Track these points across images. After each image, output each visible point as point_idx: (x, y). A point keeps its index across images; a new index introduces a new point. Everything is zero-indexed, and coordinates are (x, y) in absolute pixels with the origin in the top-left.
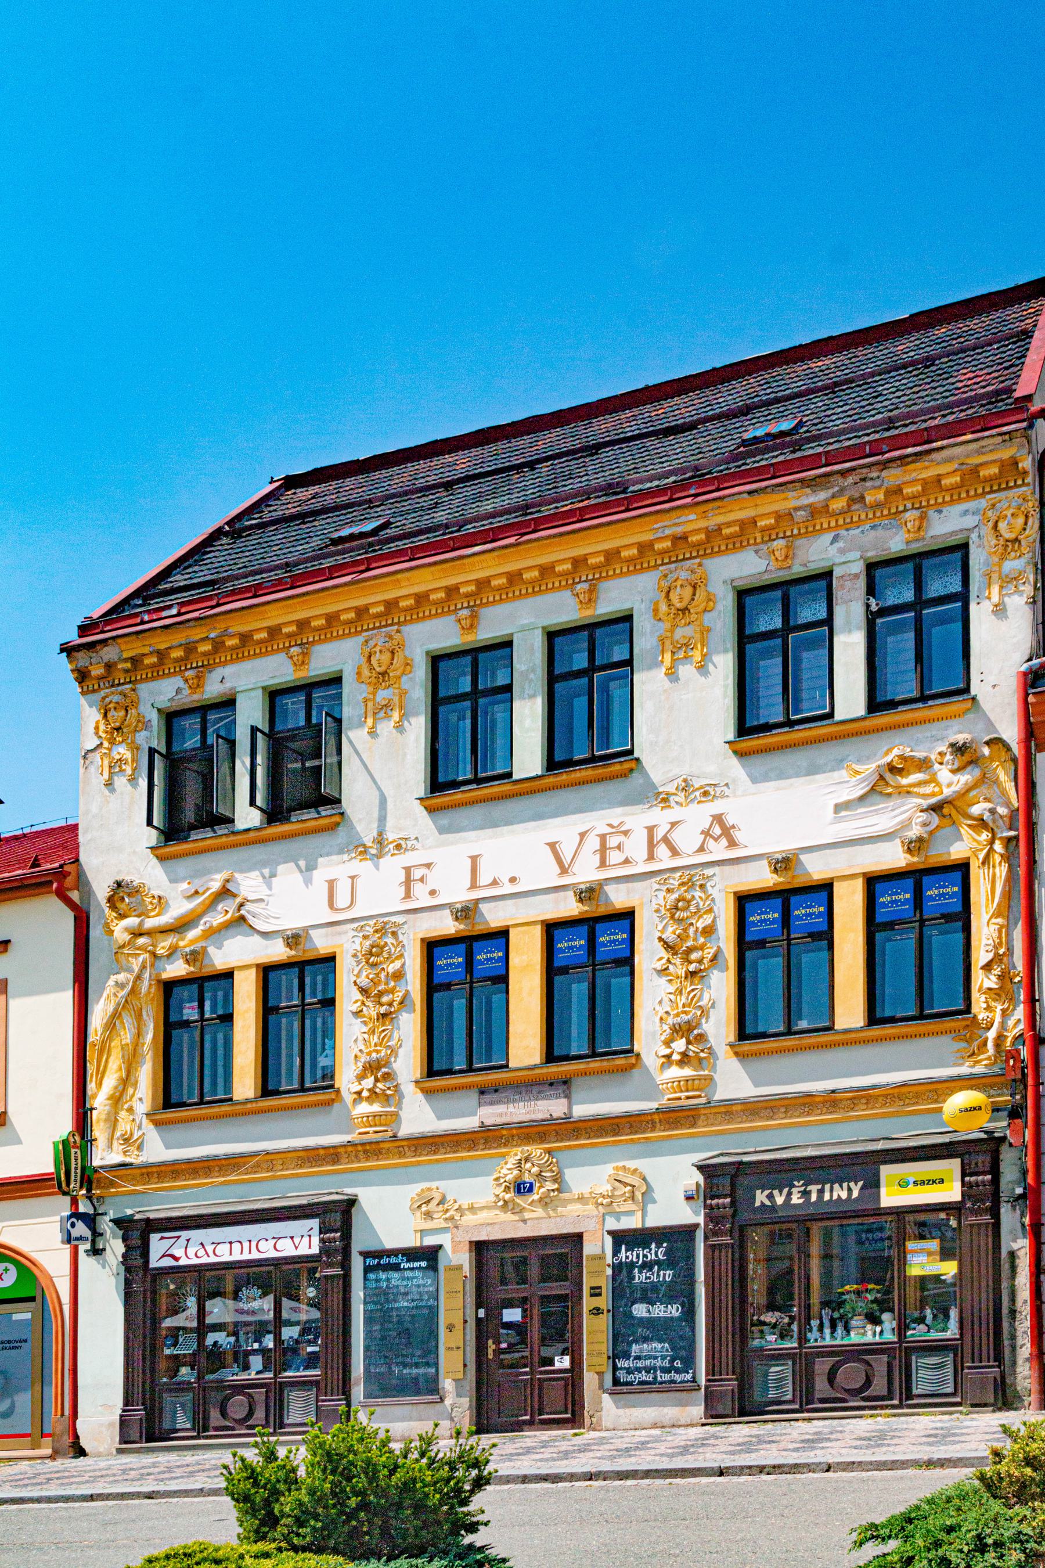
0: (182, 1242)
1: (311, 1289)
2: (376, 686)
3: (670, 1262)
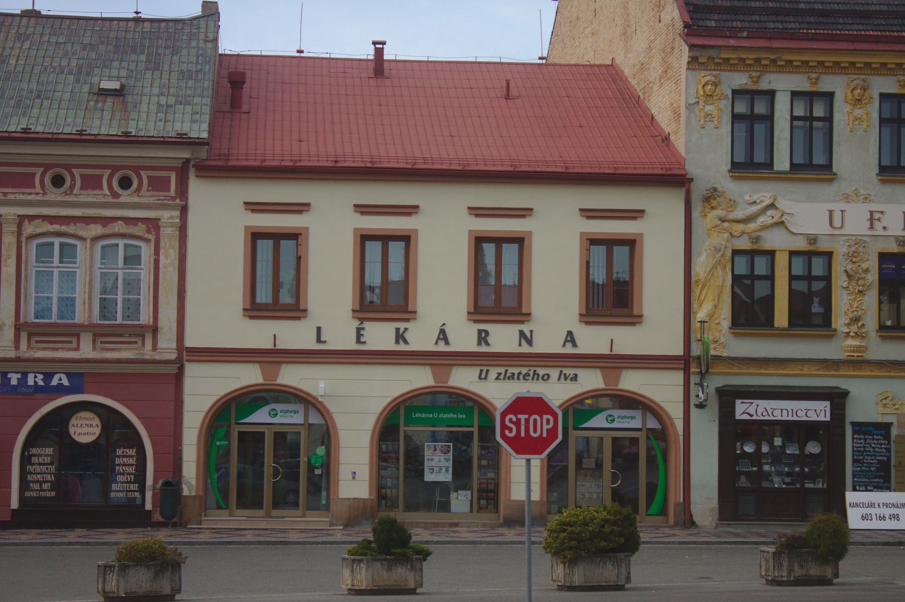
0: (754, 406)
1: (780, 439)
2: (854, 105)
3: (31, 456)
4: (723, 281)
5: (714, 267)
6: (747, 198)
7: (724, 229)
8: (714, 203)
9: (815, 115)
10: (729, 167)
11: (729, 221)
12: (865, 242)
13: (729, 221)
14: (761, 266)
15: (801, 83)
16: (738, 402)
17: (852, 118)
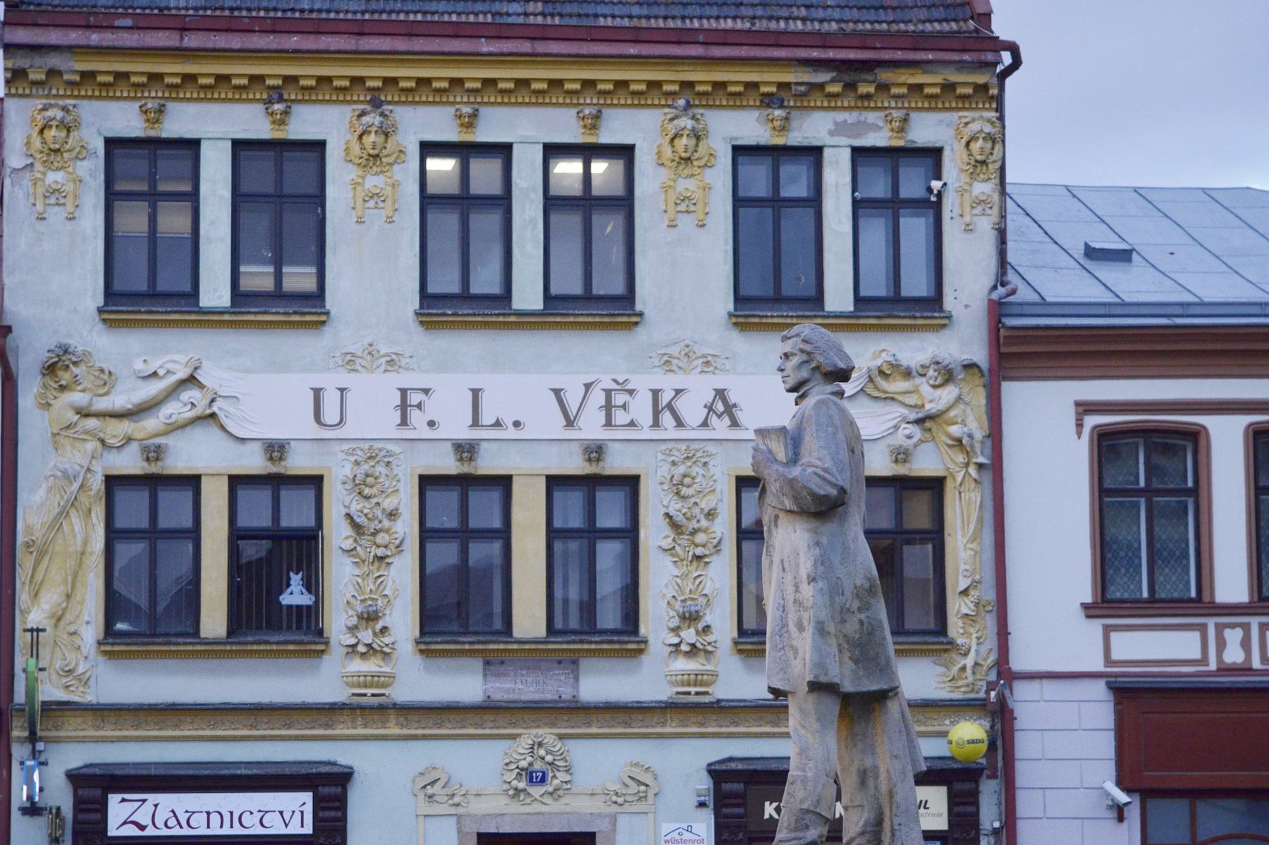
0: (148, 807)
4: (85, 543)
5: (63, 513)
6: (139, 365)
7: (87, 432)
8: (65, 377)
9: (904, 193)
10: (100, 301)
11: (98, 415)
12: (390, 454)
13: (98, 415)
14: (484, 511)
15: (252, 121)
16: (114, 799)
17: (360, 193)
